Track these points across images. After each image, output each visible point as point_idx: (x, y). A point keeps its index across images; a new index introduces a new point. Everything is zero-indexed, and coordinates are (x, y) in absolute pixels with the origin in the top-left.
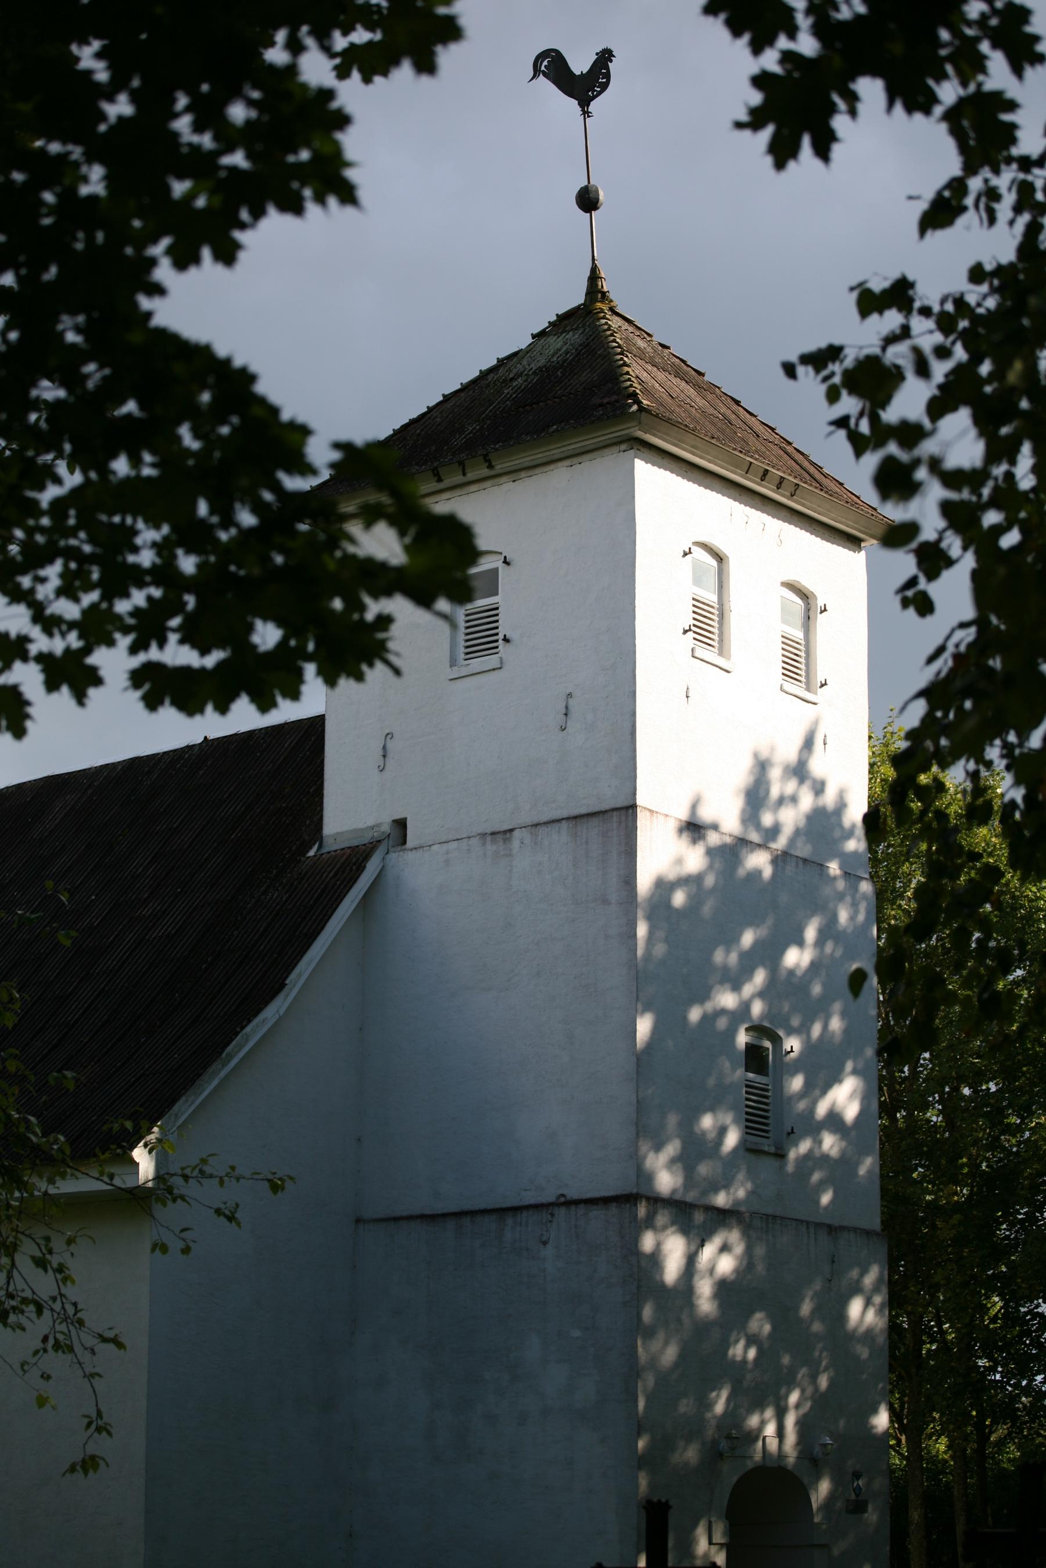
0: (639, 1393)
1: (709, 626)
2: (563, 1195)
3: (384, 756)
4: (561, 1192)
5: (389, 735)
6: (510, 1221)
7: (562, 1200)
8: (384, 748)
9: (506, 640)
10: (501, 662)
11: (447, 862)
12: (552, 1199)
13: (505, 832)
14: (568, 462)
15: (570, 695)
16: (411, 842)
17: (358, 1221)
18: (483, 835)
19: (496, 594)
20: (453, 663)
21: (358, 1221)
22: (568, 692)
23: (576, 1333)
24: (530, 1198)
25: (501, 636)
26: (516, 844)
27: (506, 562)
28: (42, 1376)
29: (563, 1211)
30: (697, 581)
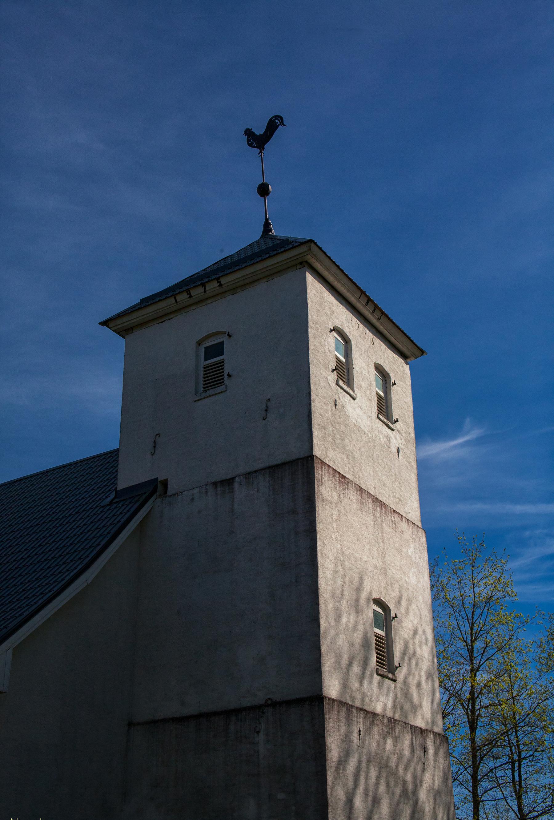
0: (425, 652)
1: (344, 372)
2: (270, 699)
3: (155, 447)
4: (269, 697)
5: (158, 435)
6: (233, 718)
7: (269, 702)
8: (155, 442)
9: (229, 375)
10: (226, 388)
11: (193, 500)
12: (263, 702)
13: (229, 480)
14: (265, 280)
15: (269, 400)
16: (169, 493)
17: (130, 724)
18: (215, 484)
19: (223, 354)
20: (196, 393)
21: (130, 724)
22: (268, 398)
23: (281, 796)
24: (247, 702)
25: (226, 373)
26: (236, 485)
27: (229, 336)
28: (165, 484)
29: (270, 709)
30: (337, 349)
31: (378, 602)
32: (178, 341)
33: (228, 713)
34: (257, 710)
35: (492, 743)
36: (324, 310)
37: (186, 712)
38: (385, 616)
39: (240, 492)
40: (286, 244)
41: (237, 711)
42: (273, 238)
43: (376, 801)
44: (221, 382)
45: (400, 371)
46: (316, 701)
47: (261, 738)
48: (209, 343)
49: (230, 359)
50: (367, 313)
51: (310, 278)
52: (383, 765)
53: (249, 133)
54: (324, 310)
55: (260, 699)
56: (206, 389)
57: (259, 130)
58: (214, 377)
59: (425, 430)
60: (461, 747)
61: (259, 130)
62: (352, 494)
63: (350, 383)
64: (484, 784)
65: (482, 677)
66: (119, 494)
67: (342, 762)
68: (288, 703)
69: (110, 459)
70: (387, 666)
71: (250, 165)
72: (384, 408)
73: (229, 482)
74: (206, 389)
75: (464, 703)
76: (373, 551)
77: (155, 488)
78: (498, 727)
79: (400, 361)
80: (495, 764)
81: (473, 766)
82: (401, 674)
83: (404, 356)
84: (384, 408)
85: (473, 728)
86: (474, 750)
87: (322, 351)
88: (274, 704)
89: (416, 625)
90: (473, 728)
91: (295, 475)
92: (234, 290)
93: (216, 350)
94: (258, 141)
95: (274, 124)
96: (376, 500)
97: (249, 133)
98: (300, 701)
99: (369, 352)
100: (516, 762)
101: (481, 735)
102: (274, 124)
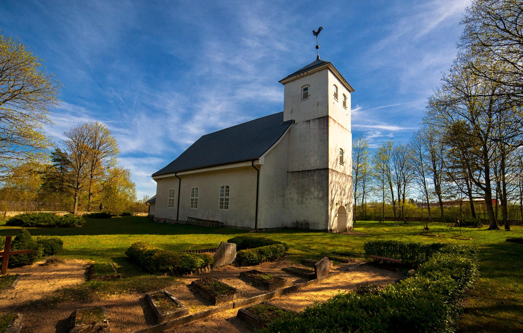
1: (336, 95)
28: (294, 121)
31: (341, 149)
32: (298, 85)
33: (308, 171)
34: (315, 170)
35: (360, 178)
36: (332, 80)
37: (299, 170)
38: (342, 152)
39: (312, 124)
40: (323, 63)
41: (310, 170)
42: (320, 60)
43: (337, 191)
44: (307, 97)
45: (348, 95)
46: (328, 169)
47: (315, 176)
48: (304, 87)
49: (310, 92)
50: (342, 81)
51: (329, 73)
52: (339, 183)
53: (314, 31)
54: (332, 80)
55: (315, 168)
56: (304, 98)
57: (316, 31)
58: (306, 96)
59: (353, 107)
60: (354, 178)
61: (316, 31)
62: (337, 124)
63: (337, 98)
64: (357, 186)
65: (360, 165)
66: (284, 123)
67: (331, 183)
68: (321, 169)
69: (280, 115)
70: (342, 162)
71: (313, 41)
72: (344, 104)
73: (309, 121)
74: (304, 98)
75: (356, 171)
76: (340, 139)
77: (292, 122)
78: (362, 175)
79: (349, 93)
80: (360, 182)
81: (356, 182)
82: (344, 164)
83: (350, 91)
84: (344, 104)
85: (357, 175)
86: (357, 179)
87: (331, 90)
88: (318, 170)
89: (348, 157)
90: (357, 175)
91: (324, 120)
92: (310, 74)
93: (306, 89)
94: (316, 34)
95: (320, 30)
96: (341, 126)
97: (314, 31)
98: (324, 169)
99: (342, 90)
100: (364, 182)
101: (358, 176)
102: (320, 30)
